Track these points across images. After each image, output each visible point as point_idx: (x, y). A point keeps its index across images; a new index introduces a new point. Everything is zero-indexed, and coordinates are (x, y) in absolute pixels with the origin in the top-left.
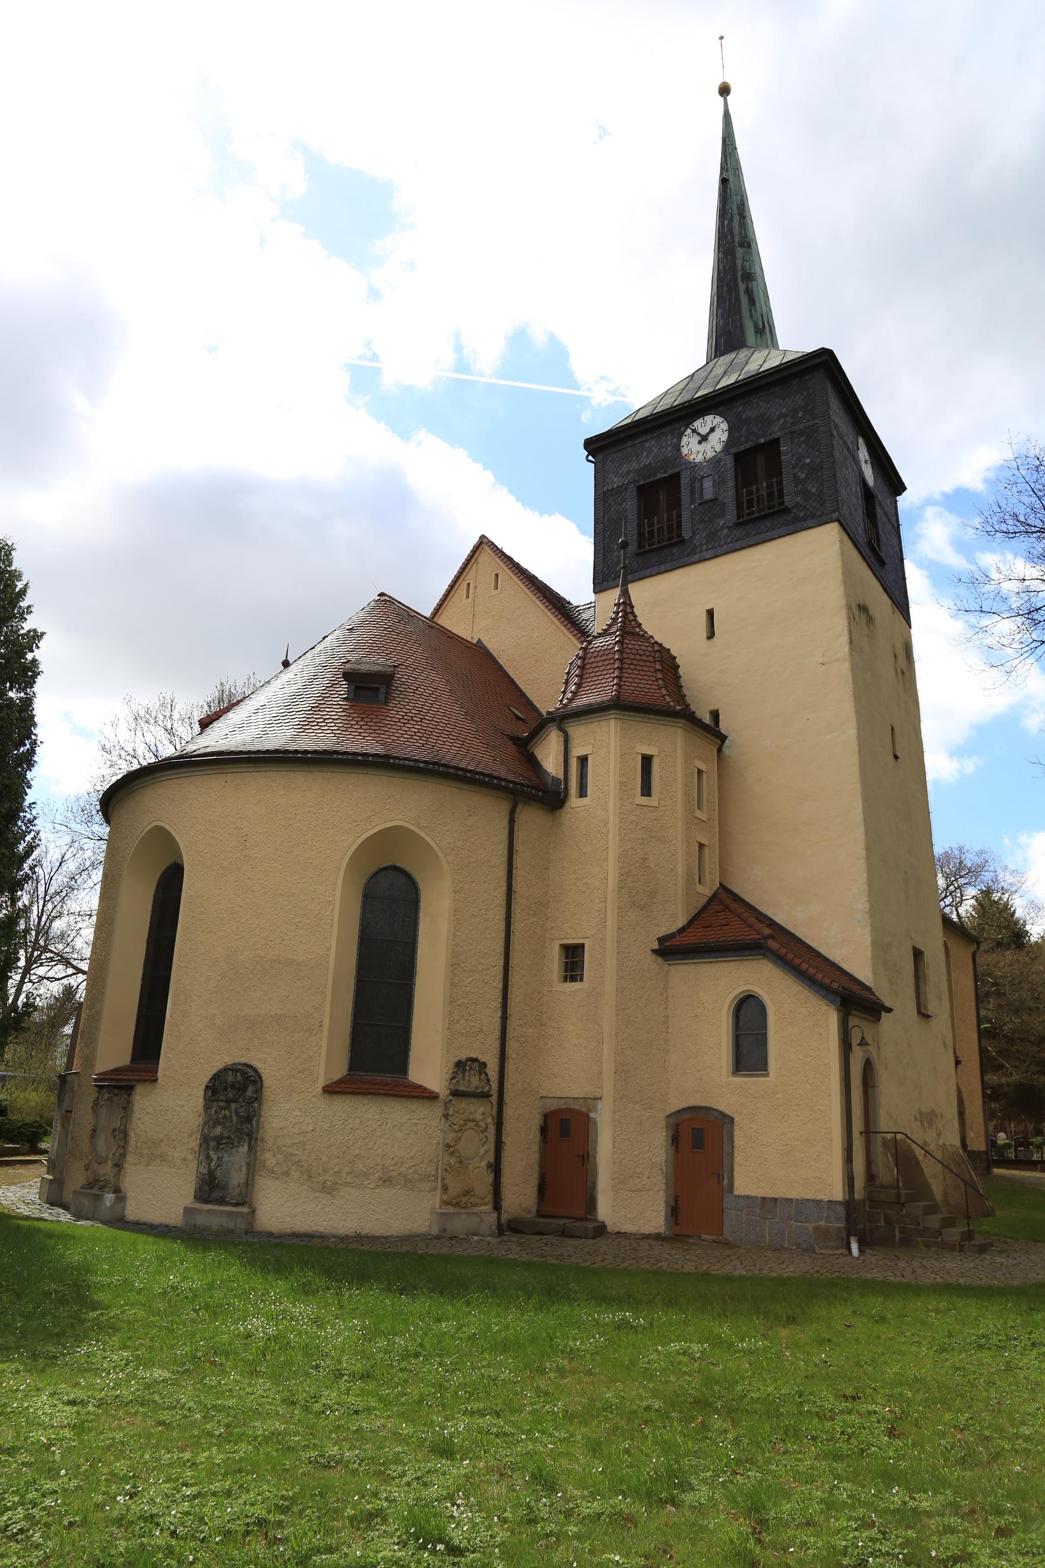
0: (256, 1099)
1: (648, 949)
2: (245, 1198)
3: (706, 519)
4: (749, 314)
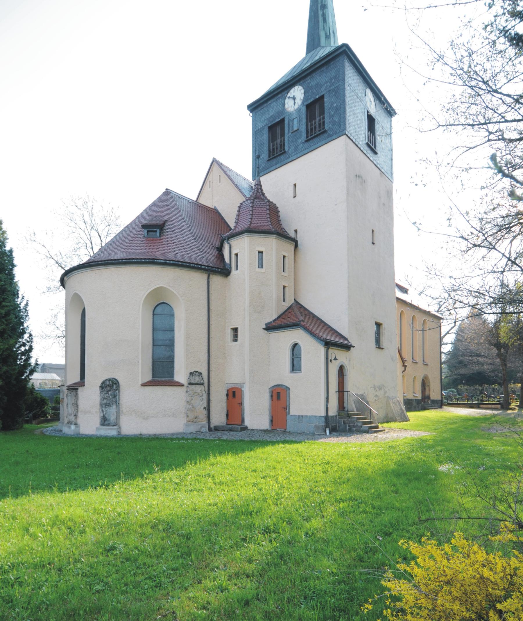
0: (117, 390)
1: (262, 328)
2: (116, 424)
3: (294, 140)
4: (323, 28)
